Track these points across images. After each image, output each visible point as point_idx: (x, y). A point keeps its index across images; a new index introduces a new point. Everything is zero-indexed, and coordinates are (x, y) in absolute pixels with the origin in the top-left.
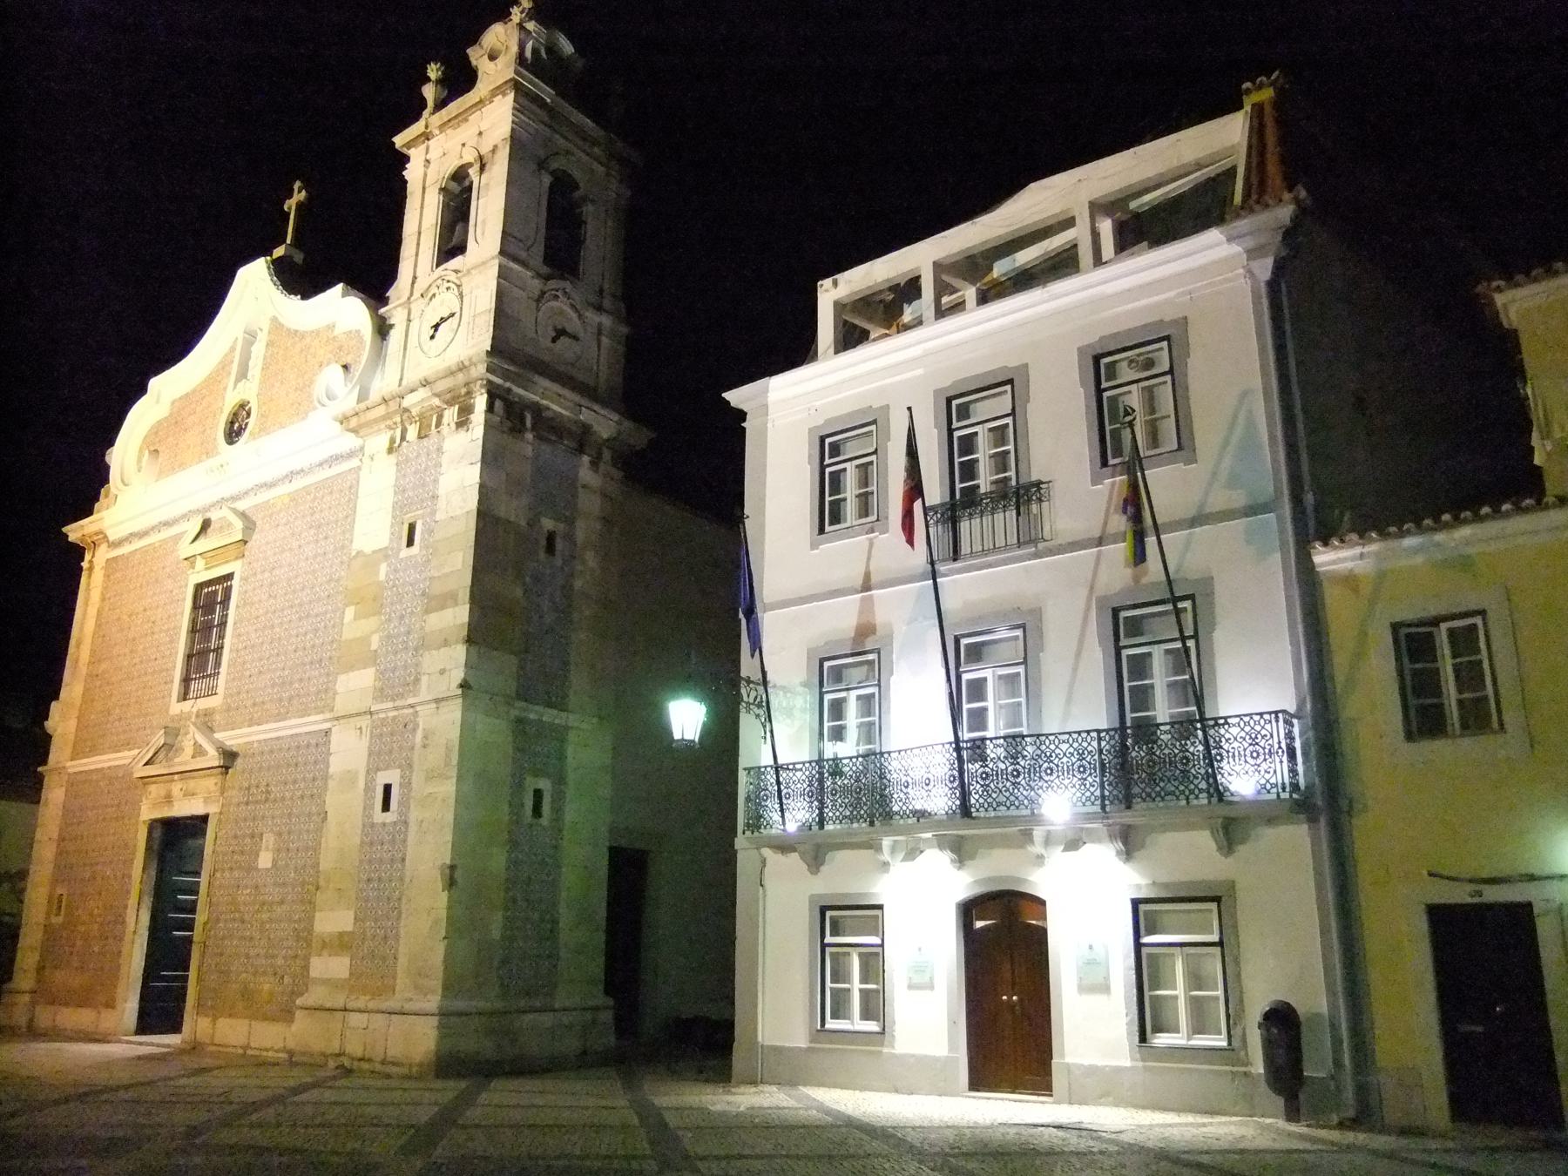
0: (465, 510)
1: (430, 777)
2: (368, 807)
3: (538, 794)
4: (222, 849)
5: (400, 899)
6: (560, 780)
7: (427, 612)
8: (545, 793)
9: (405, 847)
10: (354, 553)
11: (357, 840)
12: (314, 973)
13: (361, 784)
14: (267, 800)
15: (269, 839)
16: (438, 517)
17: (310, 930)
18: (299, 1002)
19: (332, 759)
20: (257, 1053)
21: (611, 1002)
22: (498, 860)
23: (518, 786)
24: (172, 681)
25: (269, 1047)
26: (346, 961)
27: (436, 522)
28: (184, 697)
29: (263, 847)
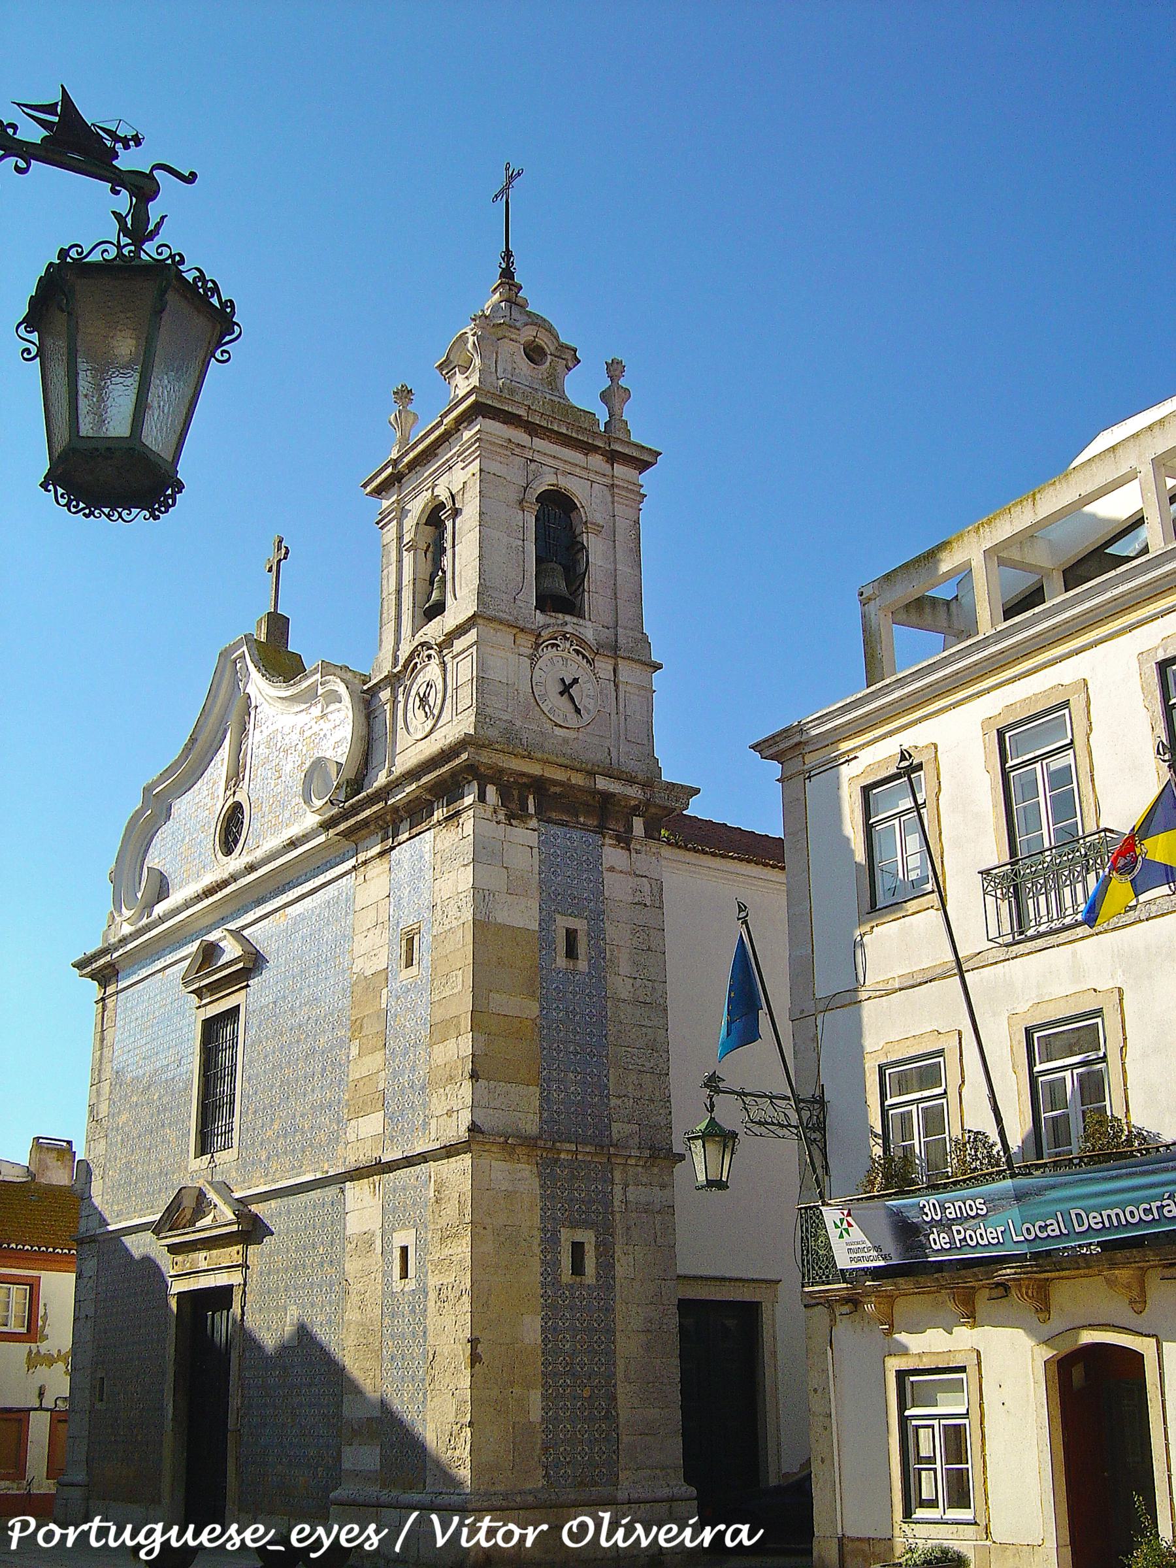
3: (578, 1249)
6: (605, 1233)
8: (587, 1247)
9: (425, 1318)
12: (346, 1465)
17: (339, 1415)
20: (362, 857)
21: (693, 1491)
22: (531, 1329)
23: (550, 1241)
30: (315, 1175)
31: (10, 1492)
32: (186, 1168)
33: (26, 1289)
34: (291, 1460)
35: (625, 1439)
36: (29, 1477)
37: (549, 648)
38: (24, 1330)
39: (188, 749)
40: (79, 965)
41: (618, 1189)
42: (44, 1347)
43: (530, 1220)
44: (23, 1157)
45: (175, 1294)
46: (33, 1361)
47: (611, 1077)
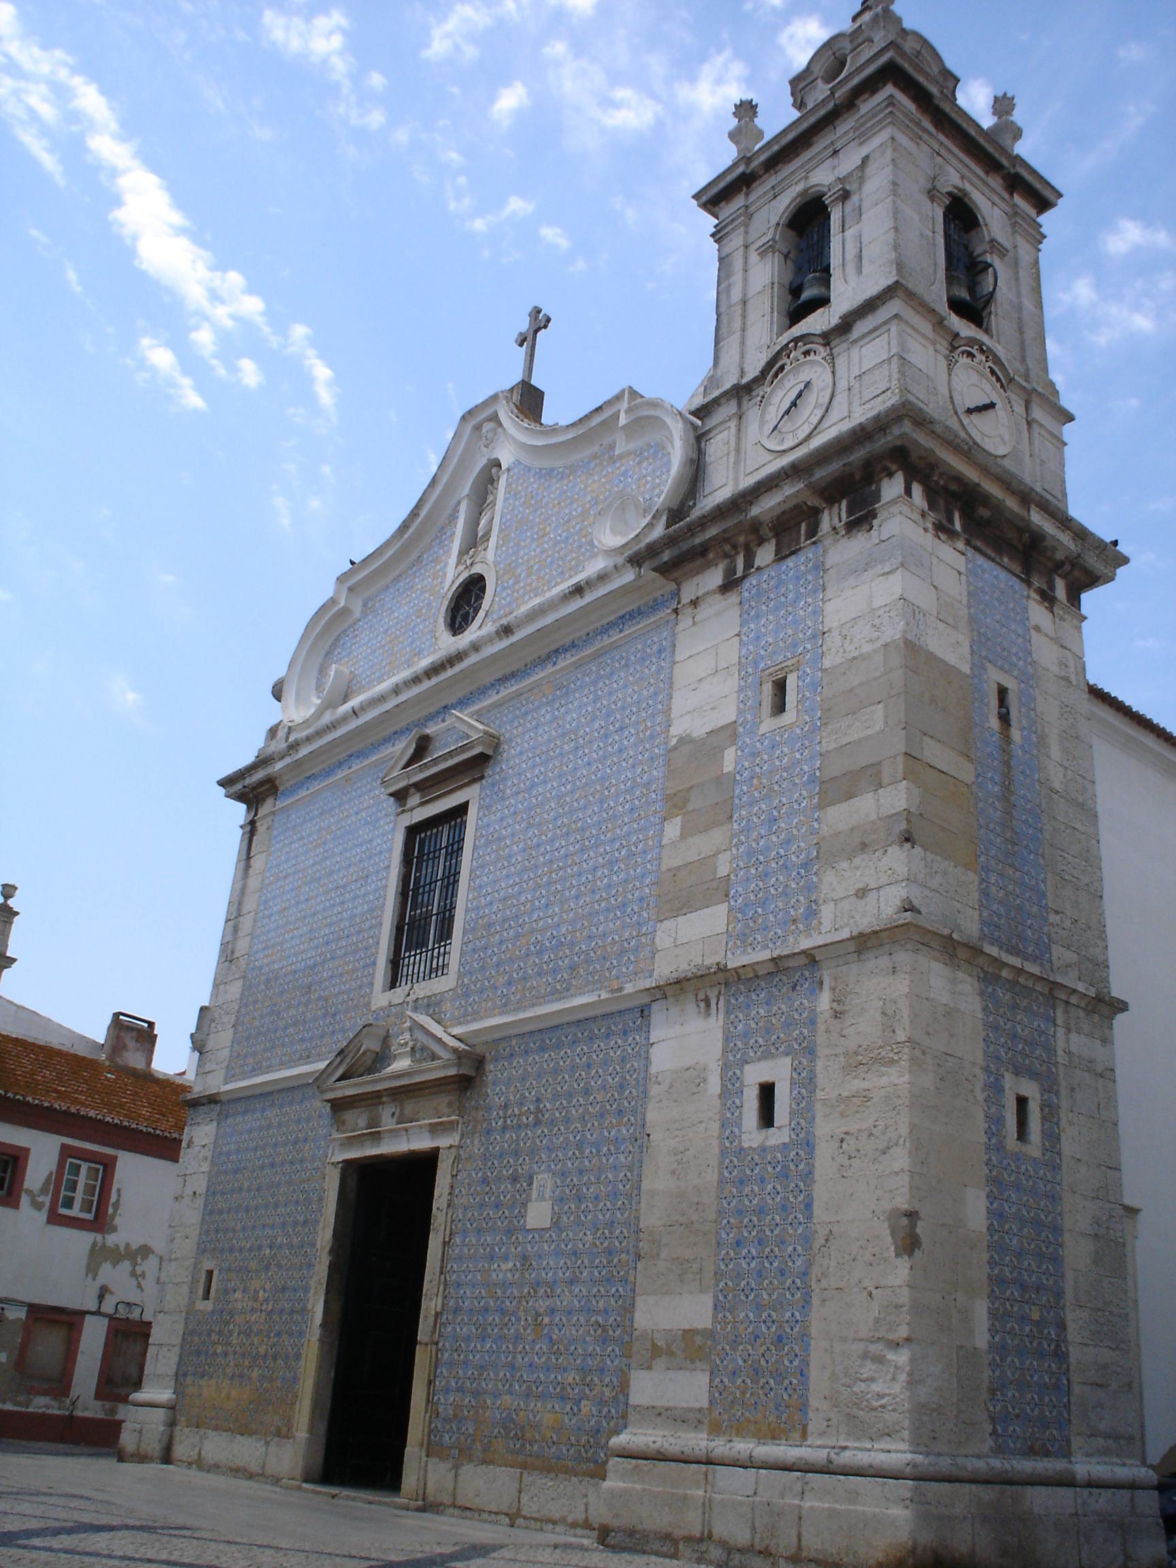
0: (879, 644)
1: (856, 1063)
2: (729, 1125)
3: (1022, 1102)
4: (464, 1201)
5: (805, 1274)
6: (1049, 1085)
7: (821, 807)
10: (674, 741)
11: (712, 1177)
13: (714, 1085)
14: (538, 1123)
15: (544, 1181)
16: (827, 663)
18: (620, 1440)
19: (654, 1051)
23: (995, 1087)
24: (374, 964)
25: (557, 1516)
26: (704, 1378)
27: (824, 671)
28: (393, 984)
29: (534, 1194)
30: (600, 996)
31: (49, 1411)
32: (368, 1005)
33: (98, 1170)
34: (529, 1388)
35: (1076, 1389)
36: (74, 1392)
37: (965, 356)
38: (90, 1217)
39: (404, 527)
40: (225, 783)
41: (1061, 1032)
42: (111, 1239)
43: (972, 1052)
44: (98, 1032)
45: (338, 1163)
46: (98, 1256)
47: (1049, 883)
